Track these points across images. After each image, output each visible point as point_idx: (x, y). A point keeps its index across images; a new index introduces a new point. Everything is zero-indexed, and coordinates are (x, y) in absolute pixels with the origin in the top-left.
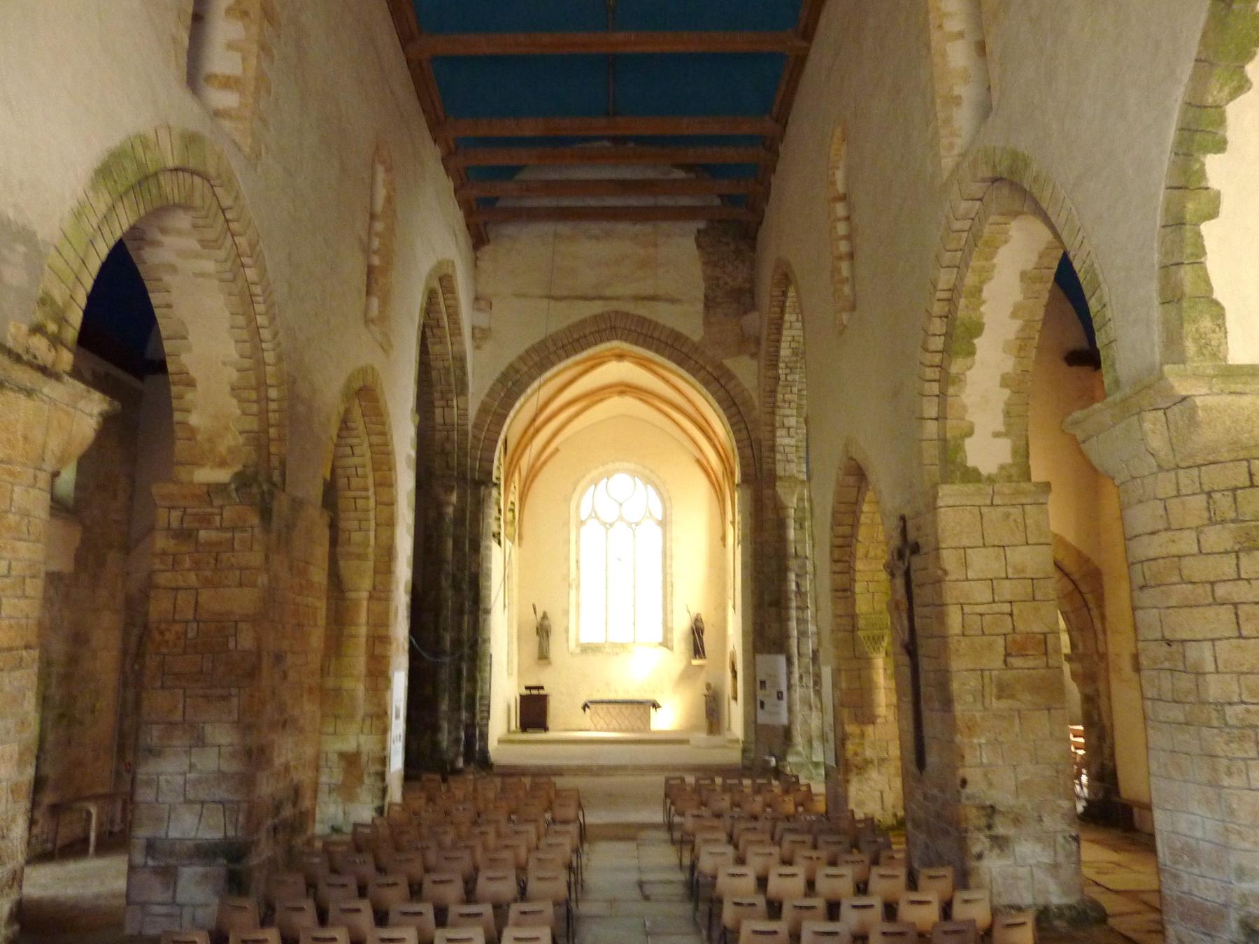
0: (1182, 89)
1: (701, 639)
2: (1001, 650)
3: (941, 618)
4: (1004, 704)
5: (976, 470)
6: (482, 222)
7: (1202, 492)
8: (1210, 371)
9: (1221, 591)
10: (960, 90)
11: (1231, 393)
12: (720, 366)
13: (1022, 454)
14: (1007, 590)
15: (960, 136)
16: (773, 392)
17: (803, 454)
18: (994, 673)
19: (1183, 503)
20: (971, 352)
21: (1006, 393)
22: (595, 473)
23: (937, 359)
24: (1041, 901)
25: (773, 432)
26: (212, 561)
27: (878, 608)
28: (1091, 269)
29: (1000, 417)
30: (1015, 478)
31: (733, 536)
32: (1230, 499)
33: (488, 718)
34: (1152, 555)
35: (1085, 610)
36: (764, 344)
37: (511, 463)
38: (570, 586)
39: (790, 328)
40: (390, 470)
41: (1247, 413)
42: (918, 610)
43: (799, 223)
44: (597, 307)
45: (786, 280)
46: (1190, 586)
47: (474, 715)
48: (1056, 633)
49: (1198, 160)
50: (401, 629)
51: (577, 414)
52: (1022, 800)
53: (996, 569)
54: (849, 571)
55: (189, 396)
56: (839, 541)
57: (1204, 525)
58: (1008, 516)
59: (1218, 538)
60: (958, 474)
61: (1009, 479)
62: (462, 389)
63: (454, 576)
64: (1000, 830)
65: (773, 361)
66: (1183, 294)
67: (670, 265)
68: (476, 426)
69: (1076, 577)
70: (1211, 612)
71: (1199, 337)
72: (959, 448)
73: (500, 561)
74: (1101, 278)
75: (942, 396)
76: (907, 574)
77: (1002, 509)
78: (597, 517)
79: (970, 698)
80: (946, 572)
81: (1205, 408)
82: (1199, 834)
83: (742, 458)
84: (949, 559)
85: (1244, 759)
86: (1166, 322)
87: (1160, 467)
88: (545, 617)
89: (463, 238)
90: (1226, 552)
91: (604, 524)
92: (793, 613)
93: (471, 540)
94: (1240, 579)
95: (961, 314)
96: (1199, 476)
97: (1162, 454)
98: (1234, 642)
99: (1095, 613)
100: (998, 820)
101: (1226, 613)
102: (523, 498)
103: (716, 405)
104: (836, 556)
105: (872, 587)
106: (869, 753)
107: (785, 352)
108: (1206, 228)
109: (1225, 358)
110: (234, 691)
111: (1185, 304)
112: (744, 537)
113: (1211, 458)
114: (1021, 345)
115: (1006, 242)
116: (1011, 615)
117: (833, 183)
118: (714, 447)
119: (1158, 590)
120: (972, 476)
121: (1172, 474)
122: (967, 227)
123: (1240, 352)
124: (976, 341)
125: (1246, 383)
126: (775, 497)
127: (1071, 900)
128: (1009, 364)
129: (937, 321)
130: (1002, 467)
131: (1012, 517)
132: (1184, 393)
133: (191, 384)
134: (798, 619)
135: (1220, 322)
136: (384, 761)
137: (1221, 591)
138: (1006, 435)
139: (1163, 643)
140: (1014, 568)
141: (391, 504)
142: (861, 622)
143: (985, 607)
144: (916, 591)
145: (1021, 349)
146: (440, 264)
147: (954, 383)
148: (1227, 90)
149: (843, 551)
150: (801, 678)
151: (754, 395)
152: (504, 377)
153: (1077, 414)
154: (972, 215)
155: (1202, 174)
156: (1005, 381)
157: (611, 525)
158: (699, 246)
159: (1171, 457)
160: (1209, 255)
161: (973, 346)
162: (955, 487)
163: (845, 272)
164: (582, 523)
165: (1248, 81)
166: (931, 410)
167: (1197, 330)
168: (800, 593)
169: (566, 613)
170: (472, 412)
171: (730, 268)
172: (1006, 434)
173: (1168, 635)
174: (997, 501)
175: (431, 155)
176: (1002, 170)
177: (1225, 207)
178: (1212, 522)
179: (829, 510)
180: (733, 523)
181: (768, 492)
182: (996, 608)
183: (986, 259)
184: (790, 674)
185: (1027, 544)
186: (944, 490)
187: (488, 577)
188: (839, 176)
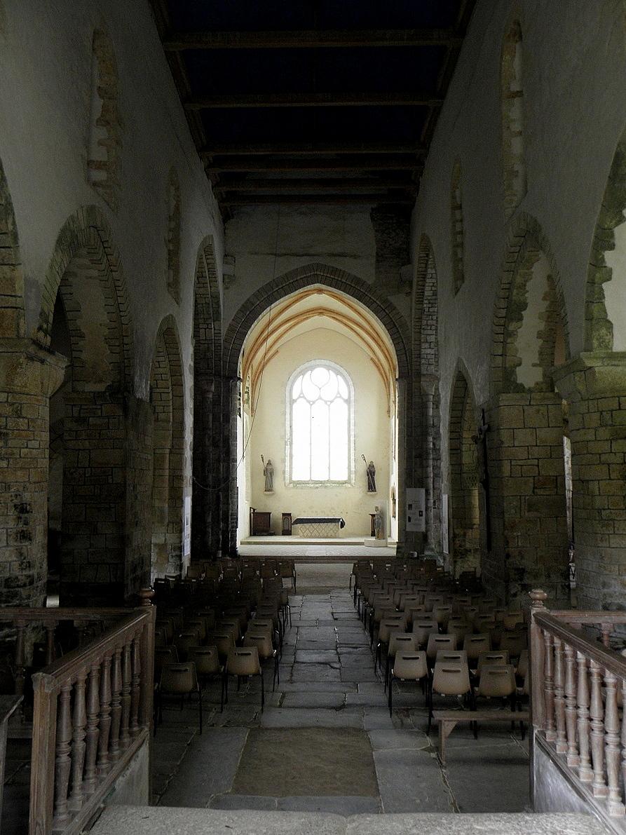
0: (597, 217)
2: (532, 485)
6: (230, 208)
9: (603, 458)
11: (612, 365)
12: (386, 301)
14: (536, 452)
18: (527, 498)
20: (521, 319)
21: (540, 342)
22: (302, 367)
23: (502, 322)
26: (98, 435)
37: (247, 362)
38: (286, 442)
40: (181, 376)
43: (433, 221)
44: (305, 261)
46: (591, 455)
50: (188, 472)
51: (291, 328)
52: (539, 566)
54: (460, 438)
55: (81, 343)
58: (538, 411)
62: (217, 316)
63: (214, 438)
64: (526, 581)
67: (358, 231)
68: (225, 341)
71: (600, 338)
72: (513, 372)
73: (242, 425)
75: (504, 343)
78: (304, 397)
79: (513, 511)
81: (599, 372)
82: (590, 569)
84: (505, 435)
85: (608, 535)
88: (269, 463)
89: (218, 217)
91: (309, 402)
92: (431, 462)
98: (607, 481)
101: (605, 468)
102: (254, 385)
106: (468, 546)
107: (428, 293)
109: (611, 348)
110: (112, 505)
113: (603, 396)
116: (538, 466)
118: (382, 351)
119: (578, 456)
120: (520, 389)
121: (586, 402)
122: (517, 251)
133: (82, 336)
136: (181, 548)
137: (603, 458)
141: (182, 396)
142: (465, 469)
145: (548, 317)
146: (203, 243)
147: (510, 336)
150: (434, 502)
152: (244, 308)
155: (603, 260)
156: (539, 335)
157: (314, 402)
158: (372, 219)
164: (294, 401)
169: (284, 461)
170: (224, 331)
172: (539, 365)
175: (198, 166)
178: (601, 426)
182: (529, 462)
183: (528, 269)
184: (427, 500)
185: (549, 427)
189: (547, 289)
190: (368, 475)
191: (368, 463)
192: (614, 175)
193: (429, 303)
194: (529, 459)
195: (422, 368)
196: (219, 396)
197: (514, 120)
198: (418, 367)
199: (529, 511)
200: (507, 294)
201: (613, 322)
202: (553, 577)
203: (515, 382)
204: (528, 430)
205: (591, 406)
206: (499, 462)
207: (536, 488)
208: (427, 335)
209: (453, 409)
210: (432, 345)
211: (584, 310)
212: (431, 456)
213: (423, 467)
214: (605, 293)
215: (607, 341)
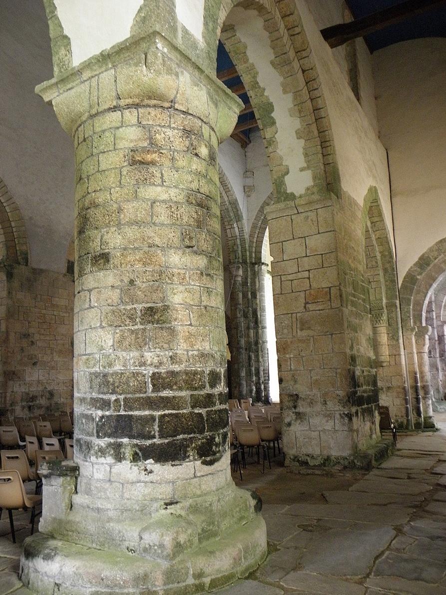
2: (303, 301)
4: (305, 333)
5: (292, 194)
14: (306, 263)
24: (325, 453)
33: (269, 380)
47: (259, 379)
62: (239, 218)
64: (300, 409)
68: (250, 236)
77: (304, 214)
93: (252, 293)
100: (300, 403)
116: (309, 278)
120: (292, 197)
124: (272, 115)
127: (346, 453)
128: (297, 123)
130: (308, 189)
145: (300, 112)
167: (59, 59)
170: (247, 229)
172: (308, 168)
174: (301, 210)
182: (299, 275)
185: (319, 233)
187: (263, 310)
194: (299, 272)
196: (246, 279)
199: (302, 330)
202: (330, 404)
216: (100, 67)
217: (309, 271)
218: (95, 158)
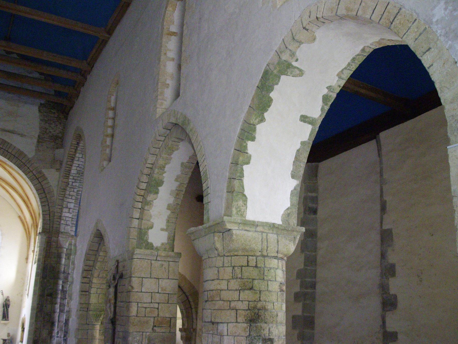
0: (244, 115)
1: (7, 310)
3: (128, 308)
5: (152, 244)
7: (231, 266)
8: (239, 221)
9: (233, 304)
10: (169, 82)
11: (245, 230)
12: (40, 172)
13: (172, 239)
15: (166, 100)
16: (65, 190)
17: (75, 223)
18: (148, 334)
19: (224, 269)
20: (157, 193)
23: (142, 193)
25: (61, 209)
27: (100, 302)
28: (205, 172)
29: (165, 222)
30: (167, 250)
31: (33, 257)
32: (240, 270)
34: (211, 289)
35: (190, 309)
36: (64, 165)
39: (78, 161)
41: (249, 238)
42: (118, 304)
45: (79, 138)
46: (223, 302)
48: (175, 318)
49: (245, 142)
53: (154, 288)
56: (87, 268)
57: (230, 279)
58: (162, 265)
59: (234, 284)
60: (144, 244)
61: (165, 249)
65: (67, 174)
66: (234, 190)
69: (188, 294)
70: (228, 312)
72: (146, 233)
74: (208, 176)
75: (142, 209)
76: (116, 287)
77: (160, 262)
80: (132, 287)
81: (236, 235)
83: (44, 220)
84: (135, 282)
86: (227, 200)
87: (219, 255)
90: (236, 290)
92: (59, 300)
94: (239, 300)
95: (155, 176)
96: (231, 260)
97: (220, 250)
98: (235, 324)
99: (194, 310)
101: (233, 313)
103: (35, 191)
104: (84, 275)
105: (99, 291)
107: (74, 171)
108: (245, 167)
111: (235, 194)
112: (39, 260)
113: (236, 253)
114: (177, 194)
115: (177, 149)
116: (158, 309)
117: (109, 101)
118: (30, 211)
120: (149, 246)
121: (222, 258)
122: (163, 140)
123: (250, 216)
124: (160, 188)
125: (251, 227)
126: (57, 242)
128: (171, 200)
129: (145, 176)
130: (163, 244)
131: (164, 266)
132: (229, 228)
134: (61, 303)
135: (245, 203)
137: (233, 304)
138: (166, 230)
139: (211, 323)
140: (162, 288)
142: (92, 307)
143: (148, 304)
144: (119, 295)
145: (177, 194)
147: (148, 205)
148: (257, 120)
149: (88, 272)
150: (58, 332)
151: (55, 190)
153: (193, 229)
154: (166, 135)
155: (246, 147)
156: (169, 207)
159: (222, 251)
160: (245, 178)
161: (158, 190)
162: (142, 250)
163: (108, 143)
165: (264, 118)
166: (136, 214)
167: (237, 205)
168: (64, 291)
171: (53, 126)
173: (213, 320)
176: (180, 122)
177: (252, 161)
179: (84, 252)
180: (33, 251)
181: (54, 239)
182: (152, 305)
183: (168, 155)
185: (168, 279)
186: (137, 251)
188: (113, 98)
189: (179, 173)
190: (4, 307)
191: (5, 298)
192: (262, 85)
193: (73, 179)
194: (151, 303)
195: (61, 227)
197: (170, 50)
198: (58, 226)
200: (150, 172)
201: (248, 197)
203: (147, 241)
204: (153, 280)
205: (226, 261)
206: (127, 304)
207: (155, 326)
208: (69, 202)
209: (87, 259)
210: (71, 210)
211: (226, 184)
212: (59, 296)
213: (52, 303)
214: (244, 173)
215: (242, 210)
216: (269, 230)
217: (158, 303)
218: (266, 282)
